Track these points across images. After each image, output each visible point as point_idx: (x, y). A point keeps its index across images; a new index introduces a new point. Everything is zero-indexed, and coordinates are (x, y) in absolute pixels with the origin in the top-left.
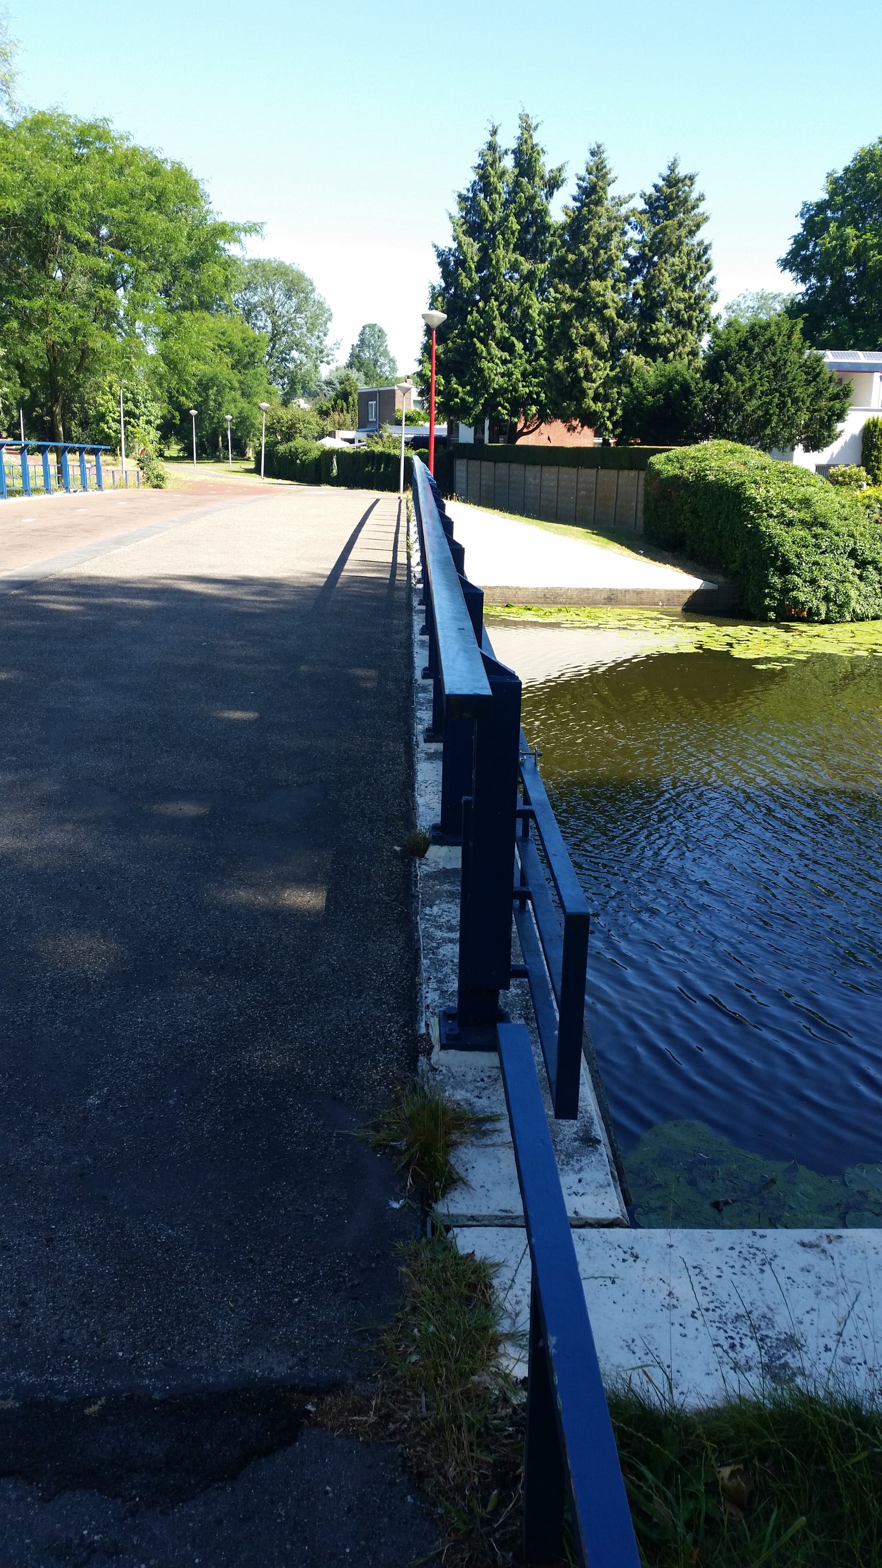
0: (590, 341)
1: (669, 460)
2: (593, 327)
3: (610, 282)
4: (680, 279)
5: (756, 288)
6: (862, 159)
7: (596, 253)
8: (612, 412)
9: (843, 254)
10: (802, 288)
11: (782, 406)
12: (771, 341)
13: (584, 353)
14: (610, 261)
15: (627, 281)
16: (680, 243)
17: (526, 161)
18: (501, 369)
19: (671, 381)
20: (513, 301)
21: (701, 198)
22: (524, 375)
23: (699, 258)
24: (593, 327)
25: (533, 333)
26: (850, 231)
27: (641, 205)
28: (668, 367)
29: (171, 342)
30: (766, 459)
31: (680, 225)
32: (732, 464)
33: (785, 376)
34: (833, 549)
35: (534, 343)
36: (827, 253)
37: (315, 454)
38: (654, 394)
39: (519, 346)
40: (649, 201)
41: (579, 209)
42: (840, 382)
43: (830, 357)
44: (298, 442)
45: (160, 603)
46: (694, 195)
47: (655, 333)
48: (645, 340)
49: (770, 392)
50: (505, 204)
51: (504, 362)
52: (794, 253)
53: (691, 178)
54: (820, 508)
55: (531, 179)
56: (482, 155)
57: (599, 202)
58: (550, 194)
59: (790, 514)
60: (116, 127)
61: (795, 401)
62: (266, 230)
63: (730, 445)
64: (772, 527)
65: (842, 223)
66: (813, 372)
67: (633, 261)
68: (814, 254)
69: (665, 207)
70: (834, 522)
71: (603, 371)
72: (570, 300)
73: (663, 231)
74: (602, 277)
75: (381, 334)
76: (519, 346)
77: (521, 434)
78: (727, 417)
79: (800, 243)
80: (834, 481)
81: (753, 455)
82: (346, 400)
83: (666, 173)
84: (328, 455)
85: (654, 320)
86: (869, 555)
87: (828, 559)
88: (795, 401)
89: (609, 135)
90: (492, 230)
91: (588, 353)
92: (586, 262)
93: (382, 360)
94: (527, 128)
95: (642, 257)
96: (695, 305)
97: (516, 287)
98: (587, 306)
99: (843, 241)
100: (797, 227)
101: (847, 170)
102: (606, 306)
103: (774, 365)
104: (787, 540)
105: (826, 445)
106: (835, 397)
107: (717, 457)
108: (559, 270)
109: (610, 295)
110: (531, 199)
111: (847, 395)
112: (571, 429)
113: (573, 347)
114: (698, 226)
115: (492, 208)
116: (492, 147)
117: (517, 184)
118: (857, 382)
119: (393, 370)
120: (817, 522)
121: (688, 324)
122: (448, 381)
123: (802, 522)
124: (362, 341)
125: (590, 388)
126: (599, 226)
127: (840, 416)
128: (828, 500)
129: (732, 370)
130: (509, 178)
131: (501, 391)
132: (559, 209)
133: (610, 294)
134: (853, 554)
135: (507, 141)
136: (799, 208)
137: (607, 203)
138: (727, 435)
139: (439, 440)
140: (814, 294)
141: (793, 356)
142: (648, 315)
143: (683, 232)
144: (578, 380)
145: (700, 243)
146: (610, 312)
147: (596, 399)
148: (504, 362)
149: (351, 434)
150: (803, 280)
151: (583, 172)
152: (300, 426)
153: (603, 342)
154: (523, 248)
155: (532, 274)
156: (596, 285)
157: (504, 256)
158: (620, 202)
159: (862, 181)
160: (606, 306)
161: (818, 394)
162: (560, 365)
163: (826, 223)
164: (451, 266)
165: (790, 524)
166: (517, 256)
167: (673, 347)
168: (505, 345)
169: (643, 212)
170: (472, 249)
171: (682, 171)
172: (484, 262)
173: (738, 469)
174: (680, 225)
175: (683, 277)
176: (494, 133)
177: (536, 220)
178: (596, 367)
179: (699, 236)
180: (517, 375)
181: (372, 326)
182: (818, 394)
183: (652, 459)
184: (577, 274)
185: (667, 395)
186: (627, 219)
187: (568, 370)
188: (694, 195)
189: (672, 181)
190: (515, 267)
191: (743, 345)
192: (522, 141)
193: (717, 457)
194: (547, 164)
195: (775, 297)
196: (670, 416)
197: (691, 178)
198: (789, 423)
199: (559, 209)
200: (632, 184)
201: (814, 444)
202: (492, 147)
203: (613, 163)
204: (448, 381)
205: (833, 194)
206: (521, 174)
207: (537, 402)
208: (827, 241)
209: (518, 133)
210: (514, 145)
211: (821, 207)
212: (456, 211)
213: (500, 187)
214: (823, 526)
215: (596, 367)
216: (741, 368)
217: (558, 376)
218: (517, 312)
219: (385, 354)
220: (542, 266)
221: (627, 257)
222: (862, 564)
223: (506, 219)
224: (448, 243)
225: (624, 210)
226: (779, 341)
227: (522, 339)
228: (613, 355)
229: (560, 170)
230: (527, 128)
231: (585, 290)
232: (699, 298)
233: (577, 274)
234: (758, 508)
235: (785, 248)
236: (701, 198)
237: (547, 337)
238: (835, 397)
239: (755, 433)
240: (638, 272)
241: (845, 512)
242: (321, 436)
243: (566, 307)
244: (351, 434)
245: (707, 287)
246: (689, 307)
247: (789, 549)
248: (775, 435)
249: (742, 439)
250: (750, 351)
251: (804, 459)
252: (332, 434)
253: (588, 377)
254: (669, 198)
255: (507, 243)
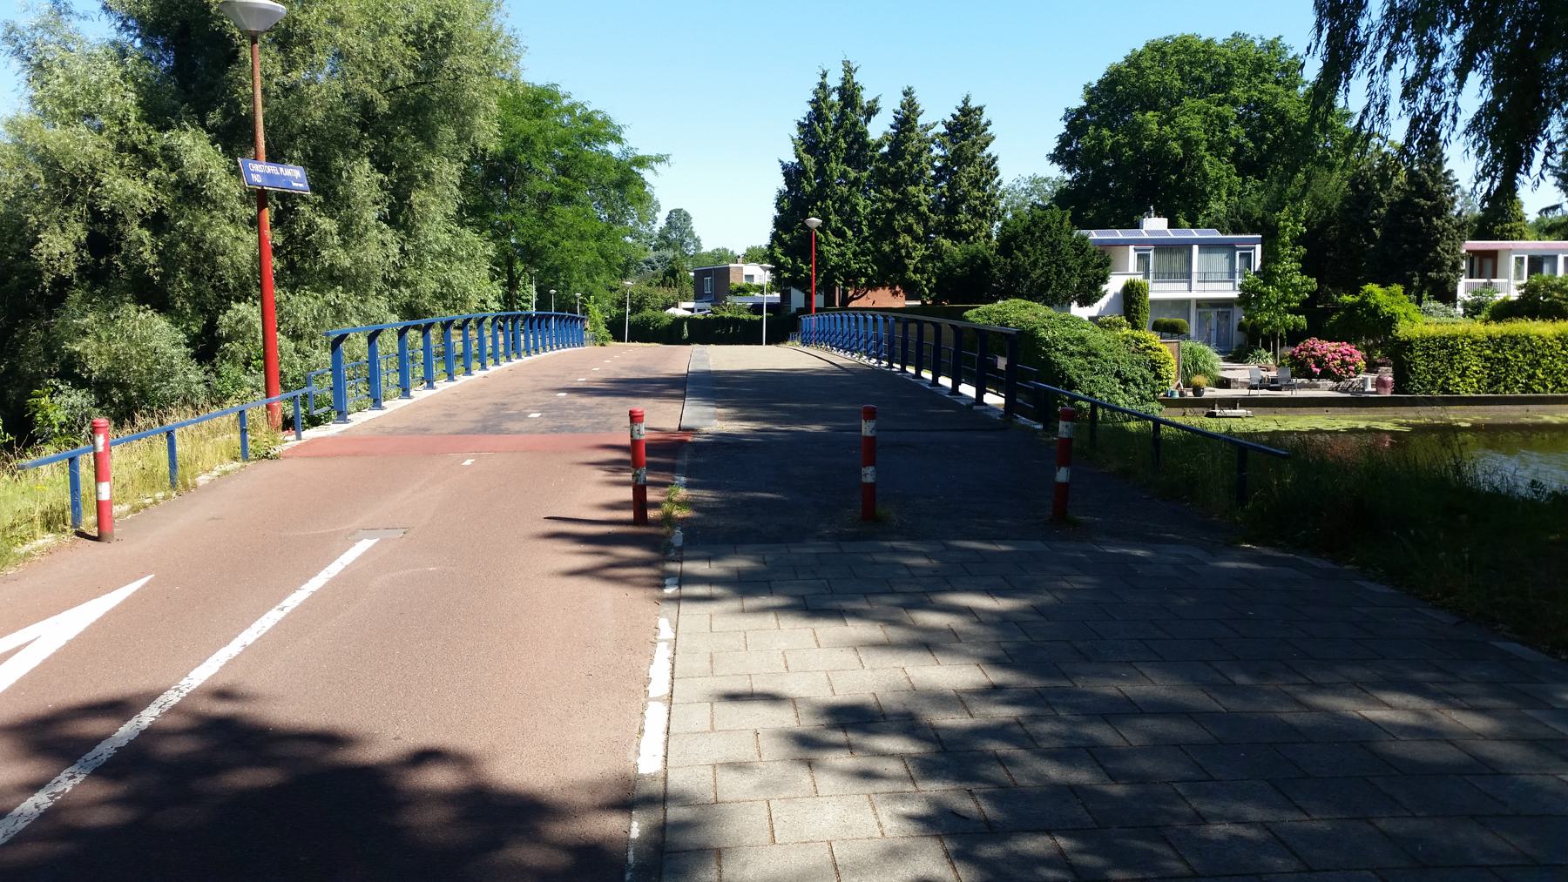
0: (909, 230)
1: (977, 315)
2: (910, 220)
3: (922, 187)
4: (975, 183)
5: (1027, 174)
6: (1111, 74)
7: (910, 166)
8: (929, 281)
9: (1101, 150)
10: (1068, 177)
11: (1059, 273)
12: (1048, 227)
13: (905, 239)
14: (922, 172)
15: (935, 185)
16: (974, 156)
17: (849, 94)
18: (836, 251)
19: (974, 257)
20: (844, 200)
21: (989, 123)
22: (855, 254)
23: (988, 167)
24: (910, 220)
25: (860, 223)
26: (1105, 132)
27: (942, 129)
28: (971, 248)
29: (604, 242)
30: (1051, 311)
31: (974, 143)
32: (1026, 315)
33: (1060, 253)
34: (1103, 371)
35: (861, 231)
36: (1088, 151)
37: (667, 321)
38: (961, 266)
39: (849, 233)
40: (948, 126)
41: (897, 135)
42: (1103, 252)
43: (1094, 235)
44: (648, 312)
45: (842, 359)
46: (983, 121)
47: (959, 223)
48: (951, 228)
49: (1050, 264)
50: (835, 130)
51: (839, 246)
52: (1060, 149)
53: (980, 109)
54: (1092, 344)
55: (853, 110)
56: (815, 93)
57: (912, 129)
58: (868, 120)
59: (1071, 348)
60: (562, 90)
61: (1069, 270)
62: (671, 160)
63: (1023, 302)
64: (1060, 358)
65: (1098, 126)
66: (1081, 247)
67: (938, 170)
68: (1077, 149)
69: (961, 131)
70: (1103, 353)
71: (920, 251)
72: (892, 201)
73: (960, 148)
74: (917, 185)
75: (687, 218)
76: (849, 233)
77: (852, 299)
78: (1018, 283)
79: (1064, 140)
80: (1101, 325)
81: (1042, 310)
82: (674, 276)
83: (961, 105)
84: (679, 321)
85: (957, 213)
86: (1129, 375)
87: (1100, 378)
88: (1069, 270)
89: (916, 81)
90: (825, 148)
91: (909, 239)
92: (903, 173)
93: (688, 240)
94: (849, 71)
95: (945, 167)
96: (988, 200)
97: (845, 189)
98: (905, 204)
99: (1100, 140)
100: (1061, 128)
101: (1100, 82)
102: (920, 204)
103: (1051, 244)
104: (1071, 366)
105: (1096, 301)
106: (1099, 266)
107: (1016, 311)
108: (881, 179)
109: (922, 196)
110: (855, 124)
111: (1108, 265)
112: (895, 294)
113: (897, 235)
114: (987, 144)
115: (825, 132)
116: (823, 86)
117: (843, 113)
118: (1115, 254)
119: (698, 247)
120: (1091, 353)
121: (983, 216)
122: (795, 261)
123: (1080, 353)
124: (669, 223)
125: (911, 264)
126: (912, 146)
127: (1104, 280)
128: (1098, 338)
129: (1020, 248)
130: (837, 109)
131: (837, 267)
132: (878, 128)
133: (922, 196)
134: (1118, 374)
135: (834, 81)
136: (1063, 113)
137: (918, 130)
138: (1020, 296)
139: (771, 307)
140: (1079, 180)
141: (1065, 237)
142: (952, 209)
143: (976, 148)
144: (900, 258)
145: (989, 156)
146: (924, 209)
147: (915, 272)
148: (839, 246)
149: (691, 305)
150: (1069, 171)
151: (898, 108)
152: (649, 299)
153: (919, 230)
154: (848, 161)
155: (857, 180)
156: (911, 189)
157: (836, 167)
158: (926, 128)
159: (1114, 92)
160: (920, 204)
161: (1086, 265)
162: (886, 248)
163: (1086, 124)
164: (793, 175)
165: (1072, 354)
166: (844, 167)
167: (972, 232)
168: (839, 233)
169: (945, 135)
170: (810, 162)
171: (973, 104)
172: (821, 171)
173: (1031, 318)
174: (974, 143)
175: (977, 181)
176: (824, 76)
177: (859, 138)
178: (915, 248)
179: (987, 151)
180: (849, 255)
181: (678, 211)
182: (1086, 265)
183: (966, 313)
184: (897, 182)
185: (972, 268)
186: (933, 141)
187: (893, 251)
188: (983, 121)
189: (966, 111)
190: (844, 175)
191: (1027, 230)
192: (846, 81)
193: (1016, 311)
194: (866, 97)
195: (1046, 180)
196: (975, 282)
197: (980, 109)
198: (1066, 286)
199: (878, 128)
200: (935, 114)
201: (1086, 301)
202: (823, 86)
203: (921, 99)
204: (795, 261)
205: (1090, 102)
206: (845, 106)
207: (866, 275)
208: (1086, 141)
209: (842, 75)
210: (839, 84)
211: (1080, 112)
212: (795, 134)
213: (832, 117)
214: (1096, 355)
215: (915, 248)
216: (1027, 247)
217: (885, 254)
218: (847, 208)
219: (691, 234)
220: (865, 174)
221: (933, 167)
222: (1125, 382)
223: (836, 140)
224: (791, 158)
225: (930, 134)
226: (1054, 226)
227: (851, 228)
228: (925, 239)
229: (875, 101)
230: (849, 71)
231: (904, 193)
232: (990, 196)
233: (897, 182)
234: (1047, 345)
235: (1052, 145)
236: (989, 123)
237: (871, 225)
238: (1099, 266)
239: (1038, 293)
240: (943, 178)
241: (1110, 346)
242: (667, 307)
243: (889, 205)
244: (691, 305)
245: (996, 187)
246: (984, 203)
247: (1072, 372)
248: (1055, 295)
249: (1030, 297)
250: (1033, 234)
251: (1076, 310)
252: (675, 305)
253: (909, 256)
254: (964, 124)
255: (837, 157)
